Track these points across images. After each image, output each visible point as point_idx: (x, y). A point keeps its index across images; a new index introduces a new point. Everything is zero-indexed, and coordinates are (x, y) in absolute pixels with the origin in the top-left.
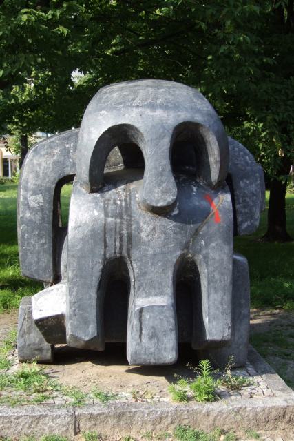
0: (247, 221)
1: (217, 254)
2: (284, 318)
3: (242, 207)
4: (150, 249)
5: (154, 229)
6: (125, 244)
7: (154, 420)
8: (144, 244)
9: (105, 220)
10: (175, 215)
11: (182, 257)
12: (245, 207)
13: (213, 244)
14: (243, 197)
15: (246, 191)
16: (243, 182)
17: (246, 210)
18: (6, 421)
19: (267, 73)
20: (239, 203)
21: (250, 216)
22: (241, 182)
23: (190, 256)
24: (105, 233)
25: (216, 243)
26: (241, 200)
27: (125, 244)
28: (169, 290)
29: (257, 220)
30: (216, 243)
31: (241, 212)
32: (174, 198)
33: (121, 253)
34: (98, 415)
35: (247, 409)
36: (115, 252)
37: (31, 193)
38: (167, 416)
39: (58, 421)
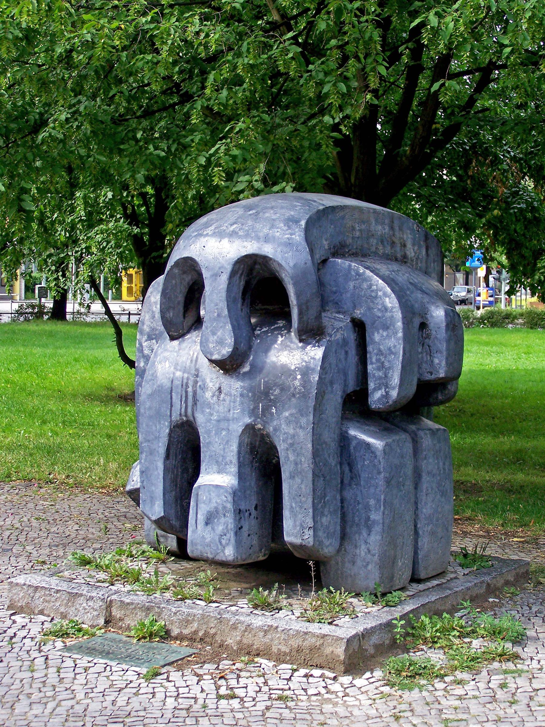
0: (380, 389)
1: (292, 427)
2: (469, 519)
3: (374, 369)
4: (215, 414)
5: (220, 388)
6: (190, 404)
7: (181, 621)
8: (209, 406)
9: (174, 373)
10: (245, 373)
11: (250, 429)
12: (379, 369)
13: (287, 414)
14: (377, 355)
15: (381, 347)
16: (378, 333)
17: (381, 374)
18: (47, 593)
19: (143, 109)
20: (372, 363)
21: (385, 383)
22: (376, 334)
23: (259, 426)
24: (171, 391)
25: (289, 412)
26: (374, 360)
27: (190, 404)
28: (234, 469)
29: (394, 388)
30: (289, 412)
31: (374, 375)
32: (231, 350)
33: (186, 416)
34: (128, 604)
35: (279, 629)
36: (180, 414)
37: (146, 337)
38: (193, 620)
39: (91, 603)
